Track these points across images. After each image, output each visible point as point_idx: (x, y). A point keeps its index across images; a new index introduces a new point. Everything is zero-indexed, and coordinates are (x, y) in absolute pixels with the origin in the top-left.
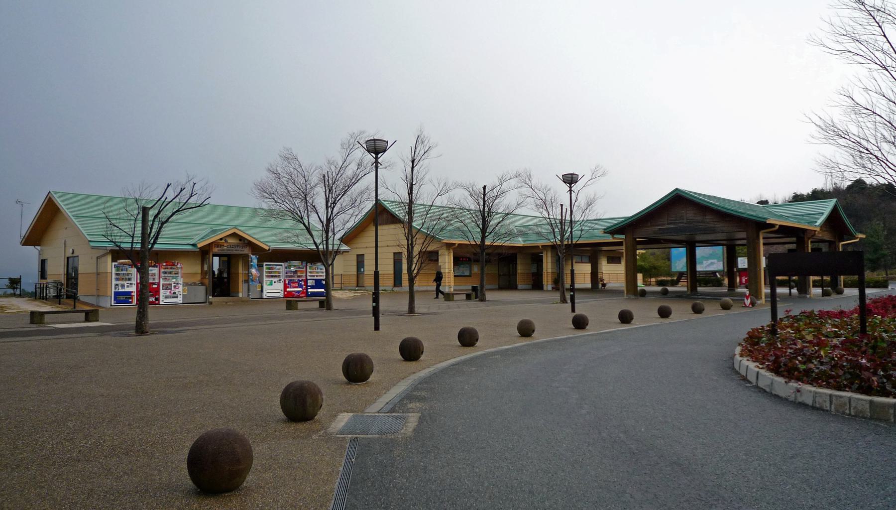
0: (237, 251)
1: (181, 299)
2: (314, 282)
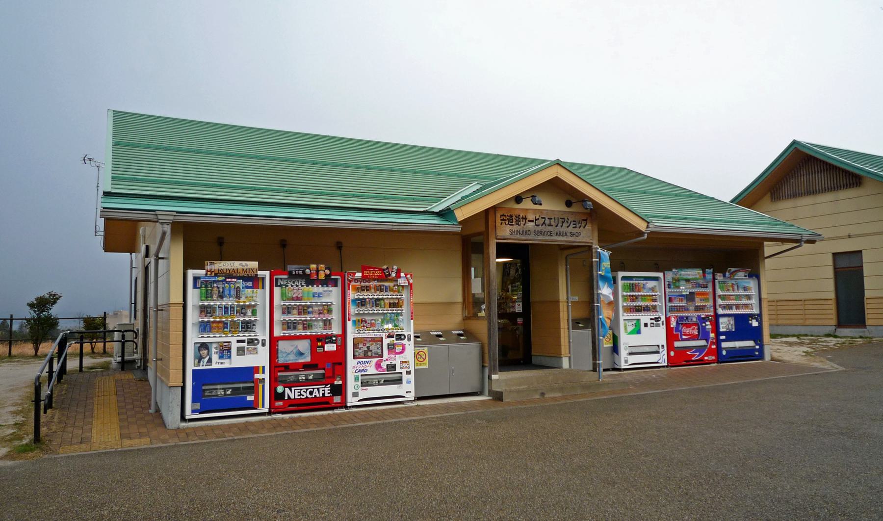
0: (559, 234)
1: (411, 387)
2: (732, 322)
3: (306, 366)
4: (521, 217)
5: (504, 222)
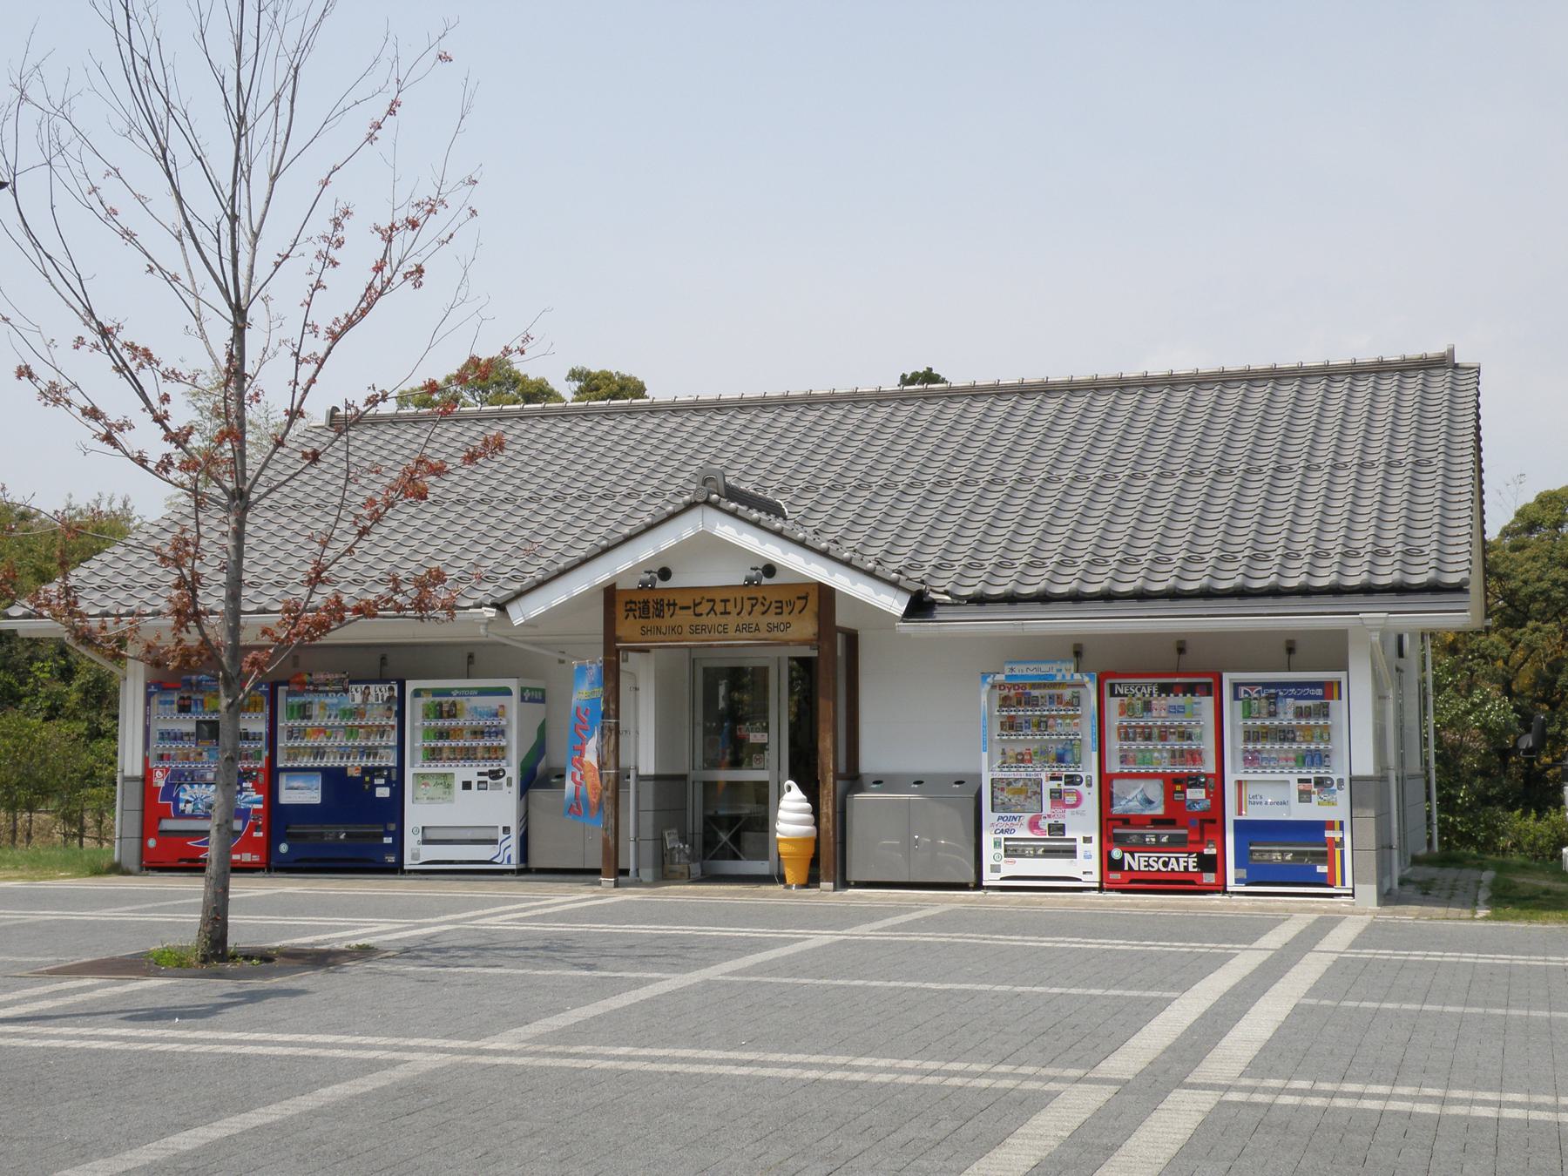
3: (1157, 822)
4: (666, 602)
5: (631, 614)
